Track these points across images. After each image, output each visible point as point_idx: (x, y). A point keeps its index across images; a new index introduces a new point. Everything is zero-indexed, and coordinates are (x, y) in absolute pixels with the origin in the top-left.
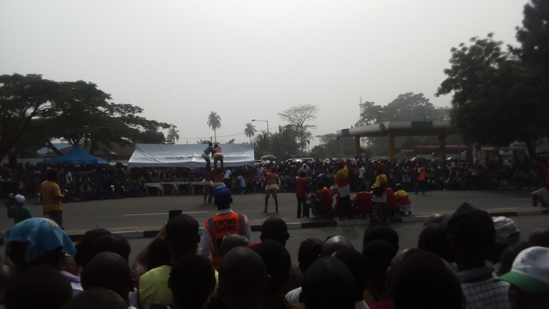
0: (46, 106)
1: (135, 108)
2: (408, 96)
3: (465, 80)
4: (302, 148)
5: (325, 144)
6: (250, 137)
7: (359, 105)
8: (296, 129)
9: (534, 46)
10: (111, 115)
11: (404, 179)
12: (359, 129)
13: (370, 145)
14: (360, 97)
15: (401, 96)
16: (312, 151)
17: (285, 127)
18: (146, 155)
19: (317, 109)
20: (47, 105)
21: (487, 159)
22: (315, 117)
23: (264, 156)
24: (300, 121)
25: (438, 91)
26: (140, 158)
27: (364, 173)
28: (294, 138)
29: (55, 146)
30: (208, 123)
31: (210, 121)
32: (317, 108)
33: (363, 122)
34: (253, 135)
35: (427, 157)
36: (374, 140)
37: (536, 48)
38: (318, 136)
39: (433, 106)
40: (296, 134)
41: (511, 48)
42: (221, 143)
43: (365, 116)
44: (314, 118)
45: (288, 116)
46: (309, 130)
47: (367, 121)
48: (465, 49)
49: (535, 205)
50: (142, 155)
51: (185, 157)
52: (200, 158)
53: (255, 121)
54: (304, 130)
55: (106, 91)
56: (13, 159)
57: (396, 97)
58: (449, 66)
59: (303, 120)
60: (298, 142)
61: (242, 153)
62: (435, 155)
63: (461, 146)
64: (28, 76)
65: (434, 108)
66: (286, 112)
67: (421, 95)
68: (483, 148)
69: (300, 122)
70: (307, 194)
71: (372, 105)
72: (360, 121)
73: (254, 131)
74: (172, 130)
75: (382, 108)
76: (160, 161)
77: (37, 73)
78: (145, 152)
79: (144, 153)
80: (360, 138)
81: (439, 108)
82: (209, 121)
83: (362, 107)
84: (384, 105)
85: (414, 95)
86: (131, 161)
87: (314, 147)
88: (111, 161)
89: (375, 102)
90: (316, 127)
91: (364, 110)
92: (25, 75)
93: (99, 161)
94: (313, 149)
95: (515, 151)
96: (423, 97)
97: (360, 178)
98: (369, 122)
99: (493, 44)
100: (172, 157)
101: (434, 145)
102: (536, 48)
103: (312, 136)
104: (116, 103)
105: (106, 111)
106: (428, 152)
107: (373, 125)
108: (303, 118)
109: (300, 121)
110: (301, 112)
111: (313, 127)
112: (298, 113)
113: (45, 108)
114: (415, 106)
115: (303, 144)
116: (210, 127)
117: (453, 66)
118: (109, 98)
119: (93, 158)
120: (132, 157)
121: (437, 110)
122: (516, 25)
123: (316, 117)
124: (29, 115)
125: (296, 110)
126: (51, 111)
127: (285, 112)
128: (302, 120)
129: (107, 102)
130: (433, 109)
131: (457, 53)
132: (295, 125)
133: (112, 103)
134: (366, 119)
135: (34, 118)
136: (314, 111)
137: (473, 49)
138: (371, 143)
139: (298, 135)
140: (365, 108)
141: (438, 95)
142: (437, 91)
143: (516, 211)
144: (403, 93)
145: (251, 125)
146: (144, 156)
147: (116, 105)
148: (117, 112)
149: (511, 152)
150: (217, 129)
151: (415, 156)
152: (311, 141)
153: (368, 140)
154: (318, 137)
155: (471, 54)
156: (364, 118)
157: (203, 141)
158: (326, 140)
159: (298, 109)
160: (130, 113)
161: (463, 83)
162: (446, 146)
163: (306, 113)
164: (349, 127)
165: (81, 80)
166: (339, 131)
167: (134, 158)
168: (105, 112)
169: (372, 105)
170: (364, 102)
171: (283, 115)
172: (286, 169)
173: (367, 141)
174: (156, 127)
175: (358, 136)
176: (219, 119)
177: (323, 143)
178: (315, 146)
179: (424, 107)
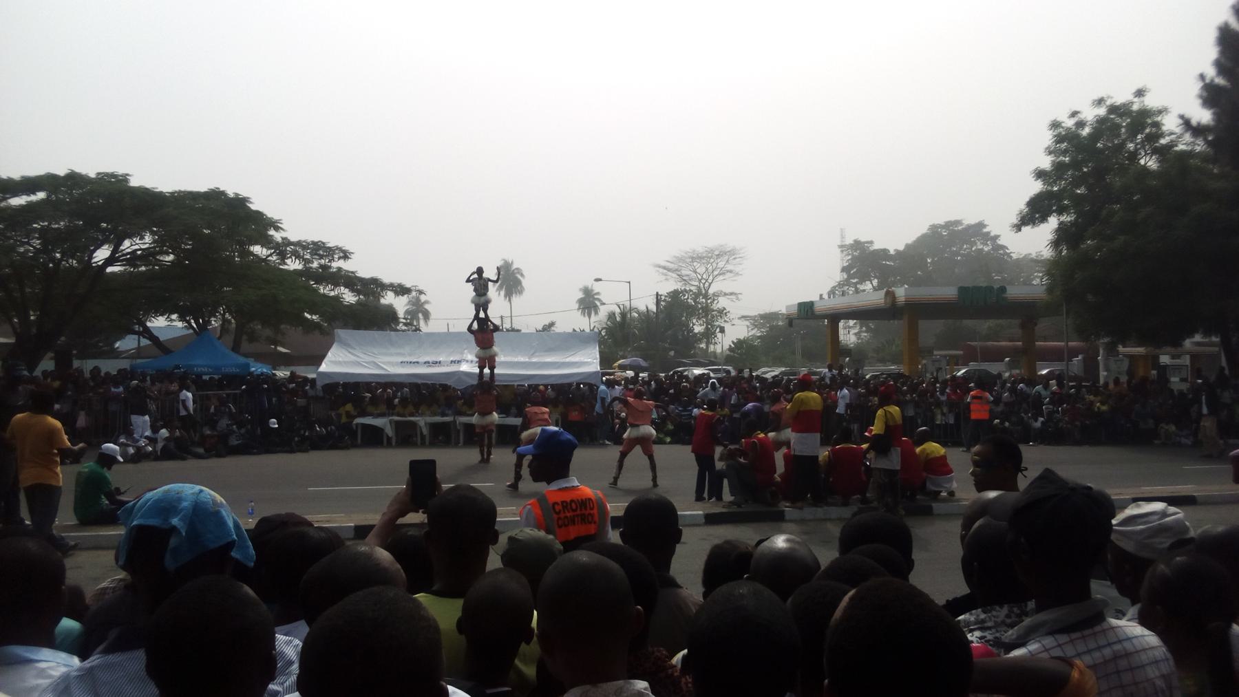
1: (334, 251)
4: (708, 344)
6: (590, 317)
8: (695, 301)
11: (939, 417)
12: (839, 303)
14: (842, 229)
15: (934, 228)
16: (728, 352)
19: (740, 256)
21: (1131, 373)
22: (737, 274)
23: (620, 362)
24: (703, 281)
26: (345, 362)
27: (848, 402)
29: (155, 333)
34: (596, 313)
35: (994, 368)
38: (744, 317)
40: (692, 311)
41: (1187, 123)
42: (523, 331)
43: (852, 272)
44: (735, 276)
45: (677, 270)
46: (722, 303)
47: (856, 284)
48: (1081, 124)
50: (350, 355)
53: (600, 282)
55: (270, 212)
58: (1046, 163)
60: (698, 329)
62: (1011, 366)
63: (1071, 344)
65: (1011, 257)
67: (981, 225)
68: (1121, 349)
71: (868, 247)
72: (840, 285)
73: (598, 303)
76: (389, 370)
77: (120, 170)
78: (355, 349)
81: (1021, 257)
86: (324, 368)
89: (874, 240)
90: (740, 296)
91: (848, 260)
92: (92, 175)
93: (253, 367)
95: (1194, 357)
96: (985, 230)
97: (839, 414)
98: (861, 287)
100: (415, 360)
101: (1010, 341)
103: (730, 316)
104: (293, 238)
105: (271, 255)
107: (870, 293)
115: (709, 335)
116: (499, 294)
117: (1053, 161)
118: (277, 229)
119: (242, 360)
124: (100, 263)
126: (148, 256)
127: (671, 263)
128: (707, 280)
132: (691, 291)
134: (854, 279)
135: (109, 269)
138: (866, 334)
141: (1018, 227)
144: (941, 220)
145: (592, 290)
146: (353, 358)
148: (294, 258)
149: (1186, 360)
150: (515, 299)
151: (965, 364)
152: (727, 327)
154: (743, 319)
155: (1097, 134)
156: (850, 277)
158: (763, 325)
161: (1078, 201)
162: (1037, 343)
163: (717, 264)
164: (814, 297)
167: (332, 362)
168: (269, 256)
169: (868, 247)
171: (664, 268)
172: (672, 391)
173: (856, 331)
175: (835, 318)
176: (519, 276)
179: (988, 253)
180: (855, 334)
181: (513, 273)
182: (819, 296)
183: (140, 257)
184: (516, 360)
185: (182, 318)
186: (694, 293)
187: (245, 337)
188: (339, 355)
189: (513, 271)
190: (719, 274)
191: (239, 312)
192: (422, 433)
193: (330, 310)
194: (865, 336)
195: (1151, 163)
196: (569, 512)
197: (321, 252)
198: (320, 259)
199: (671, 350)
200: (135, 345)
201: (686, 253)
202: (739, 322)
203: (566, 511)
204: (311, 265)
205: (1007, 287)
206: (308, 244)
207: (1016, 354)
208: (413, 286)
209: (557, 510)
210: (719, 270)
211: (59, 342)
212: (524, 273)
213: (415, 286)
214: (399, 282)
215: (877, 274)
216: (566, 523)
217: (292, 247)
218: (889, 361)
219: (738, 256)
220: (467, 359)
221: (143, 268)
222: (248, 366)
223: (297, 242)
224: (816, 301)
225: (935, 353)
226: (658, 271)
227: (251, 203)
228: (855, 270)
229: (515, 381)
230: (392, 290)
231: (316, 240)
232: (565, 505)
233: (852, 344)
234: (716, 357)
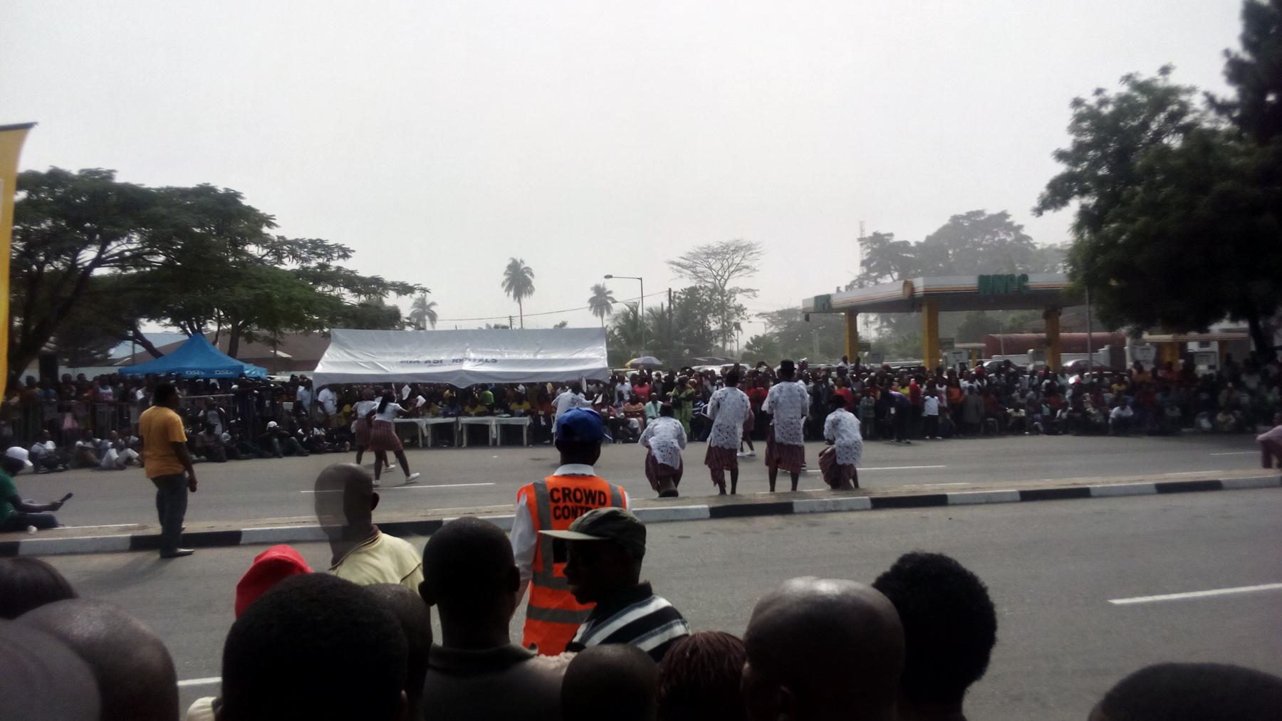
1: (332, 249)
2: (973, 218)
3: (1104, 176)
4: (724, 341)
5: (777, 331)
6: (602, 316)
7: (856, 240)
9: (1264, 95)
12: (857, 296)
14: (861, 222)
15: (956, 220)
16: (746, 350)
17: (683, 292)
18: (357, 356)
19: (757, 251)
21: (1158, 362)
22: (755, 270)
23: (634, 360)
25: (1040, 203)
26: (341, 362)
28: (704, 317)
29: (149, 339)
30: (503, 284)
31: (507, 280)
32: (760, 248)
34: (609, 312)
35: (1018, 360)
36: (894, 321)
37: (1271, 98)
38: (761, 315)
39: (1032, 242)
40: (707, 309)
41: (1211, 101)
43: (872, 265)
44: (752, 272)
45: (691, 267)
46: (739, 299)
47: (876, 278)
48: (1103, 103)
49: (1267, 464)
50: (347, 356)
51: (447, 361)
52: (481, 363)
54: (728, 300)
55: (263, 208)
58: (1066, 142)
60: (714, 326)
63: (1094, 334)
64: (83, 173)
65: (1035, 248)
66: (685, 257)
67: (1004, 215)
68: (1146, 336)
69: (719, 281)
73: (610, 302)
74: (420, 302)
75: (913, 247)
76: (388, 370)
77: (105, 167)
79: (349, 351)
80: (856, 315)
81: (1046, 247)
82: (507, 280)
83: (864, 246)
84: (916, 240)
85: (986, 217)
86: (320, 369)
88: (278, 373)
89: (893, 232)
91: (868, 253)
94: (748, 343)
95: (1223, 343)
96: (1008, 220)
98: (881, 281)
99: (1172, 92)
100: (416, 360)
101: (1034, 332)
102: (1271, 98)
106: (1020, 348)
107: (890, 285)
108: (725, 272)
109: (719, 278)
114: (990, 241)
115: (726, 332)
116: (508, 295)
117: (1075, 141)
118: (270, 225)
119: (237, 363)
120: (322, 361)
122: (1223, 47)
123: (757, 269)
124: (87, 264)
125: (711, 254)
127: (687, 259)
128: (722, 277)
129: (268, 234)
130: (1032, 250)
131: (1085, 112)
132: (705, 287)
133: (279, 237)
134: (874, 272)
135: (98, 272)
138: (886, 329)
139: (713, 312)
140: (873, 249)
141: (1039, 211)
142: (1038, 202)
143: (1220, 479)
144: (962, 211)
145: (604, 289)
146: (352, 359)
148: (291, 257)
149: (1214, 347)
150: (525, 300)
152: (743, 324)
153: (879, 322)
154: (760, 317)
155: (1119, 114)
156: (870, 270)
157: (493, 326)
158: (780, 322)
159: (715, 251)
160: (321, 260)
161: (1101, 181)
162: (1061, 334)
163: (733, 260)
164: (831, 290)
165: (206, 182)
166: (809, 300)
167: (327, 362)
168: (264, 256)
169: (888, 240)
170: (868, 234)
171: (679, 265)
175: (852, 311)
176: (529, 276)
177: (774, 329)
179: (1011, 243)
181: (522, 272)
182: (835, 289)
183: (127, 259)
184: (521, 358)
185: (175, 322)
186: (710, 290)
187: (241, 339)
189: (522, 270)
190: (736, 270)
192: (423, 435)
193: (328, 309)
194: (886, 332)
195: (1174, 141)
196: (571, 501)
197: (319, 251)
198: (318, 258)
199: (685, 348)
200: (130, 353)
202: (757, 319)
205: (1029, 275)
206: (305, 243)
208: (416, 285)
209: (556, 498)
210: (735, 266)
212: (533, 272)
213: (418, 285)
214: (401, 281)
215: (898, 267)
218: (910, 356)
219: (754, 251)
221: (134, 271)
224: (833, 295)
225: (957, 345)
228: (875, 263)
229: (521, 379)
231: (314, 238)
233: (872, 339)
234: (732, 355)
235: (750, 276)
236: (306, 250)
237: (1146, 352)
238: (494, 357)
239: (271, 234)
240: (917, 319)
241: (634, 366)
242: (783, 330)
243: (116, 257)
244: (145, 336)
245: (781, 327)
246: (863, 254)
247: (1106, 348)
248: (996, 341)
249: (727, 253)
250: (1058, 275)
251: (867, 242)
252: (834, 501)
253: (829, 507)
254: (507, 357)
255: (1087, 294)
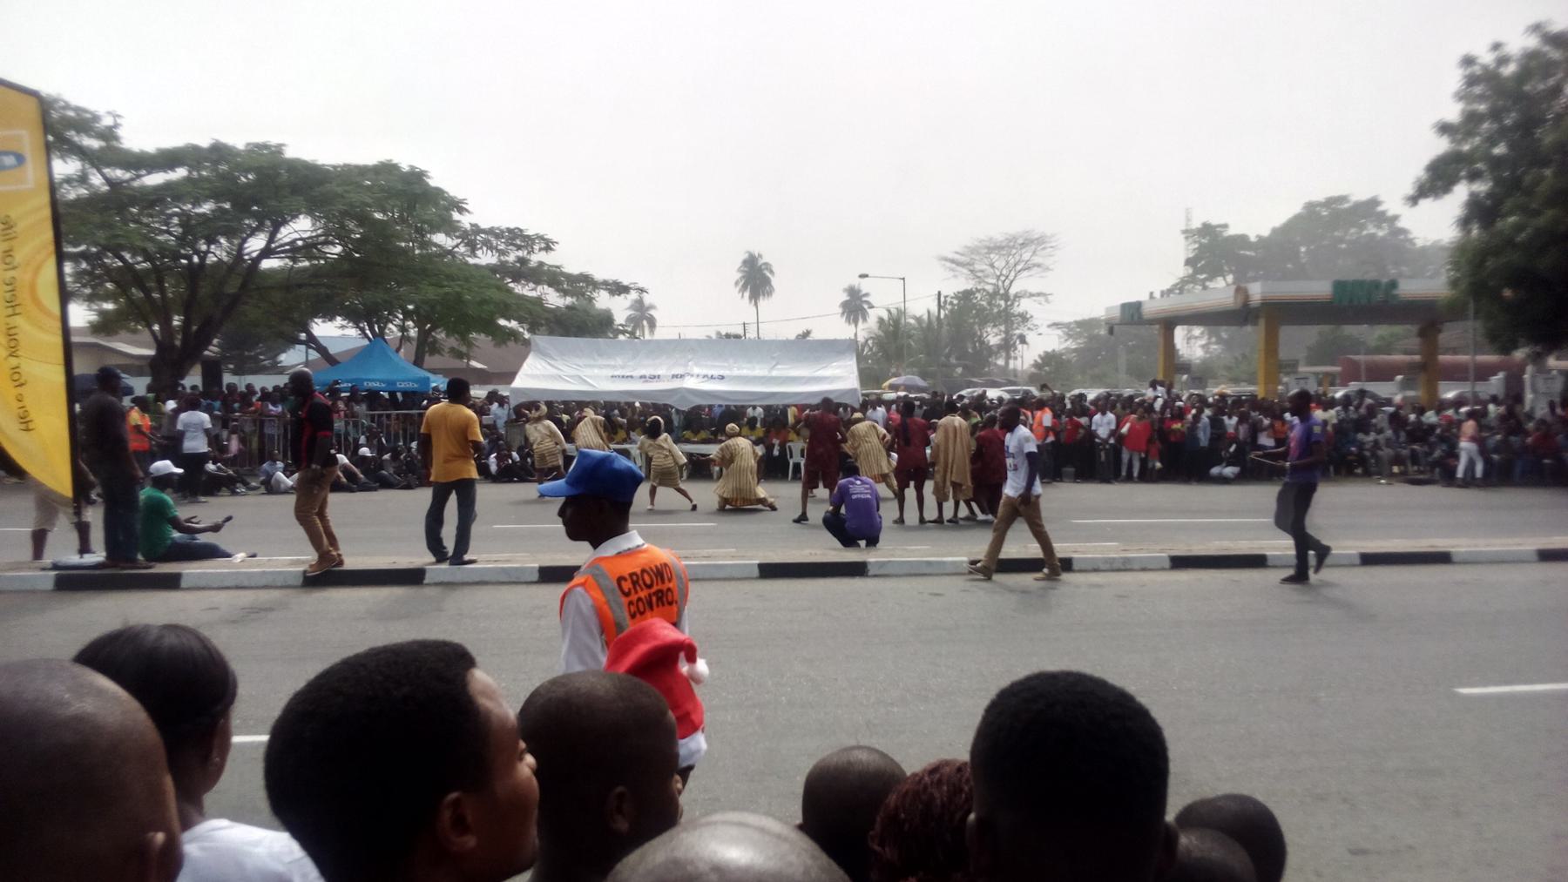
0: (296, 231)
2: (1334, 206)
4: (1008, 358)
5: (1074, 347)
6: (856, 326)
8: (990, 304)
10: (469, 256)
13: (1211, 353)
15: (1311, 208)
17: (956, 296)
18: (560, 367)
19: (1051, 245)
20: (301, 227)
22: (1048, 269)
23: (893, 380)
24: (1003, 278)
26: (543, 376)
29: (324, 343)
30: (737, 283)
31: (743, 277)
33: (1192, 285)
34: (865, 320)
35: (1382, 389)
38: (1056, 325)
39: (1411, 236)
40: (985, 318)
43: (1199, 265)
45: (968, 264)
46: (1024, 306)
48: (1503, 61)
50: (549, 367)
51: (729, 376)
52: (706, 379)
53: (867, 279)
54: (1012, 304)
55: (453, 190)
56: (212, 373)
57: (1294, 208)
58: (1453, 112)
59: (1011, 277)
60: (993, 337)
61: (824, 365)
64: (249, 148)
65: (1414, 244)
67: (1374, 202)
68: (1551, 362)
70: (394, 467)
73: (866, 306)
76: (595, 385)
77: (273, 140)
78: (556, 360)
79: (552, 362)
80: (1174, 328)
81: (1428, 244)
82: (741, 278)
83: (1190, 240)
86: (520, 382)
87: (1040, 356)
91: (1195, 249)
93: (434, 382)
96: (1380, 208)
98: (1211, 285)
100: (629, 374)
104: (484, 225)
105: (457, 246)
106: (1382, 373)
107: (1220, 291)
108: (1010, 271)
110: (1005, 252)
111: (1041, 299)
112: (997, 257)
113: (296, 236)
115: (1007, 346)
116: (743, 296)
117: (1463, 112)
118: (461, 210)
119: (423, 373)
121: (1424, 249)
123: (1051, 267)
124: (254, 255)
126: (309, 248)
127: (962, 255)
128: (1007, 277)
129: (458, 222)
132: (984, 290)
133: (472, 225)
134: (1201, 273)
135: (267, 264)
136: (1044, 249)
137: (1531, 57)
138: (1215, 347)
141: (1414, 200)
144: (1319, 196)
145: (859, 291)
146: (555, 371)
147: (484, 231)
148: (485, 248)
150: (763, 302)
151: (1344, 384)
152: (1030, 337)
155: (1525, 74)
156: (1197, 271)
159: (998, 244)
160: (520, 253)
161: (1496, 163)
163: (1021, 256)
164: (1143, 297)
167: (527, 375)
168: (453, 248)
170: (1196, 224)
171: (953, 261)
173: (1203, 342)
174: (591, 292)
175: (1168, 324)
176: (768, 274)
178: (1042, 354)
179: (1383, 239)
180: (1203, 346)
181: (760, 269)
188: (535, 367)
191: (420, 318)
197: (518, 242)
198: (517, 250)
201: (980, 242)
202: (1050, 331)
203: (638, 588)
204: (507, 258)
206: (502, 232)
207: (1412, 373)
208: (631, 284)
209: (627, 590)
211: (206, 353)
214: (614, 279)
216: (642, 610)
217: (483, 236)
220: (692, 373)
222: (427, 380)
223: (490, 229)
224: (1145, 301)
226: (944, 265)
227: (429, 178)
228: (1203, 262)
230: (606, 289)
232: (635, 579)
234: (1016, 376)
235: (1042, 277)
236: (503, 240)
237: (1302, 381)
238: (722, 372)
239: (463, 222)
240: (1254, 334)
241: (894, 388)
242: (1082, 346)
243: (287, 247)
244: (322, 341)
245: (1079, 341)
246: (1188, 250)
247: (1501, 375)
248: (1356, 364)
249: (1013, 247)
250: (1433, 284)
251: (1195, 235)
252: (1122, 558)
253: (1116, 566)
254: (736, 372)
255: (1471, 305)
